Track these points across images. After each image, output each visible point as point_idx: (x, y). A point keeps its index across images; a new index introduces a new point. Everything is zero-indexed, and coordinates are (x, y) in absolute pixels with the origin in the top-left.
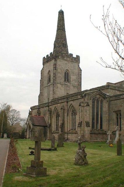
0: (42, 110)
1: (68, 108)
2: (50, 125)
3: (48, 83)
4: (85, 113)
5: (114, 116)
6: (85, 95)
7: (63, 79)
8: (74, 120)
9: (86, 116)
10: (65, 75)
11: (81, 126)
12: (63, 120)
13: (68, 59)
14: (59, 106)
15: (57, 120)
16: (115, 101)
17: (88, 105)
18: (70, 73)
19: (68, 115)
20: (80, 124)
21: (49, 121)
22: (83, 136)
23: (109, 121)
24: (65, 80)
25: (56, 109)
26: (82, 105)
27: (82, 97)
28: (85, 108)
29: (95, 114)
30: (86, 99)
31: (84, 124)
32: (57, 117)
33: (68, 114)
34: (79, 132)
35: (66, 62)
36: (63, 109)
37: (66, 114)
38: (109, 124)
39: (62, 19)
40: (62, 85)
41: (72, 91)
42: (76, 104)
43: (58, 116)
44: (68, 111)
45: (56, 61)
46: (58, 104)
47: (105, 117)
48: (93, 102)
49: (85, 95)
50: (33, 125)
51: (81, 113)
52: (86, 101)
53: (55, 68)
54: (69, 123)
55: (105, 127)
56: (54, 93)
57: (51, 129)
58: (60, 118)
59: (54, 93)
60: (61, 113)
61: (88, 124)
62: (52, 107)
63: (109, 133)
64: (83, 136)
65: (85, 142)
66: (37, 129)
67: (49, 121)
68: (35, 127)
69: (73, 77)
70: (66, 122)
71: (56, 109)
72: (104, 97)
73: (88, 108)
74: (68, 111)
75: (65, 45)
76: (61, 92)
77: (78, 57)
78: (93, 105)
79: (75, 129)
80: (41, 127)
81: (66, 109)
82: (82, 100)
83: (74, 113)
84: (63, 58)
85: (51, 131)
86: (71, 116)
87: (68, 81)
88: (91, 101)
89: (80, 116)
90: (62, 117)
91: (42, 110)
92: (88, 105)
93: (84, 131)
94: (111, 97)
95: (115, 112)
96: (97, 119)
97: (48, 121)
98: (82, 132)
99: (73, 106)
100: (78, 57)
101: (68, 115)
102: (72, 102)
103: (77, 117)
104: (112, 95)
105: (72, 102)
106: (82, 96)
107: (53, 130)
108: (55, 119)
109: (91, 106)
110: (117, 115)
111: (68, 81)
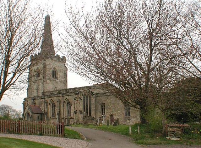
0: (37, 101)
1: (64, 101)
2: (47, 113)
3: (37, 78)
4: (79, 105)
5: (100, 107)
6: (79, 93)
7: (52, 76)
8: (69, 111)
9: (79, 106)
10: (53, 72)
11: (76, 113)
12: (60, 109)
13: (56, 59)
14: (55, 99)
15: (53, 109)
16: (101, 97)
17: (81, 100)
18: (58, 71)
19: (64, 106)
20: (75, 112)
21: (46, 110)
22: (78, 120)
23: (96, 110)
24: (53, 77)
25: (52, 101)
26: (76, 99)
27: (76, 94)
28: (79, 101)
29: (86, 106)
30: (79, 96)
31: (78, 112)
32: (52, 107)
33: (64, 105)
34: (75, 118)
35: (54, 62)
36: (59, 101)
37: (62, 105)
38: (96, 113)
39: (48, 23)
40: (51, 80)
41: (60, 87)
42: (71, 98)
43: (54, 106)
44: (64, 103)
45: (45, 60)
46: (54, 98)
47: (93, 108)
48: (84, 97)
49: (79, 93)
50: (32, 113)
51: (75, 105)
52: (79, 97)
53: (45, 67)
54: (65, 111)
55: (93, 114)
56: (44, 87)
57: (48, 116)
58: (56, 107)
59: (44, 87)
60: (57, 104)
61: (81, 112)
62: (49, 100)
63: (98, 118)
64: (78, 120)
65: (79, 124)
66: (36, 116)
67: (46, 110)
68: (34, 115)
69: (60, 74)
70: (62, 111)
71: (52, 101)
72: (92, 94)
73: (81, 102)
74: (64, 103)
75: (52, 47)
76: (50, 86)
77: (64, 58)
78: (84, 100)
79: (70, 116)
80: (39, 115)
81: (62, 101)
82: (76, 96)
83: (69, 104)
84: (51, 58)
85: (47, 117)
86: (66, 107)
87: (55, 77)
88: (83, 96)
89: (75, 106)
90: (59, 107)
91: (37, 101)
92: (81, 100)
93: (79, 117)
94: (97, 94)
95: (100, 104)
96: (87, 109)
97: (44, 109)
98: (77, 118)
99: (68, 100)
100: (64, 58)
101: (64, 106)
102: (67, 97)
103: (72, 108)
104: (98, 93)
105: (68, 96)
106: (76, 93)
107: (50, 117)
108: (52, 109)
109: (83, 100)
110: (102, 107)
111: (55, 77)
